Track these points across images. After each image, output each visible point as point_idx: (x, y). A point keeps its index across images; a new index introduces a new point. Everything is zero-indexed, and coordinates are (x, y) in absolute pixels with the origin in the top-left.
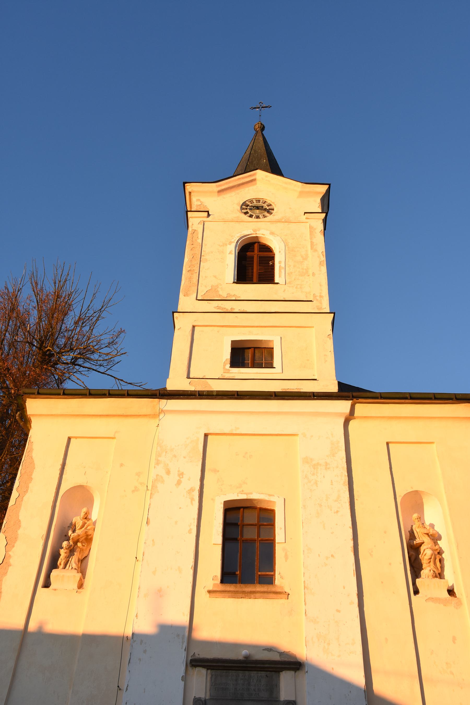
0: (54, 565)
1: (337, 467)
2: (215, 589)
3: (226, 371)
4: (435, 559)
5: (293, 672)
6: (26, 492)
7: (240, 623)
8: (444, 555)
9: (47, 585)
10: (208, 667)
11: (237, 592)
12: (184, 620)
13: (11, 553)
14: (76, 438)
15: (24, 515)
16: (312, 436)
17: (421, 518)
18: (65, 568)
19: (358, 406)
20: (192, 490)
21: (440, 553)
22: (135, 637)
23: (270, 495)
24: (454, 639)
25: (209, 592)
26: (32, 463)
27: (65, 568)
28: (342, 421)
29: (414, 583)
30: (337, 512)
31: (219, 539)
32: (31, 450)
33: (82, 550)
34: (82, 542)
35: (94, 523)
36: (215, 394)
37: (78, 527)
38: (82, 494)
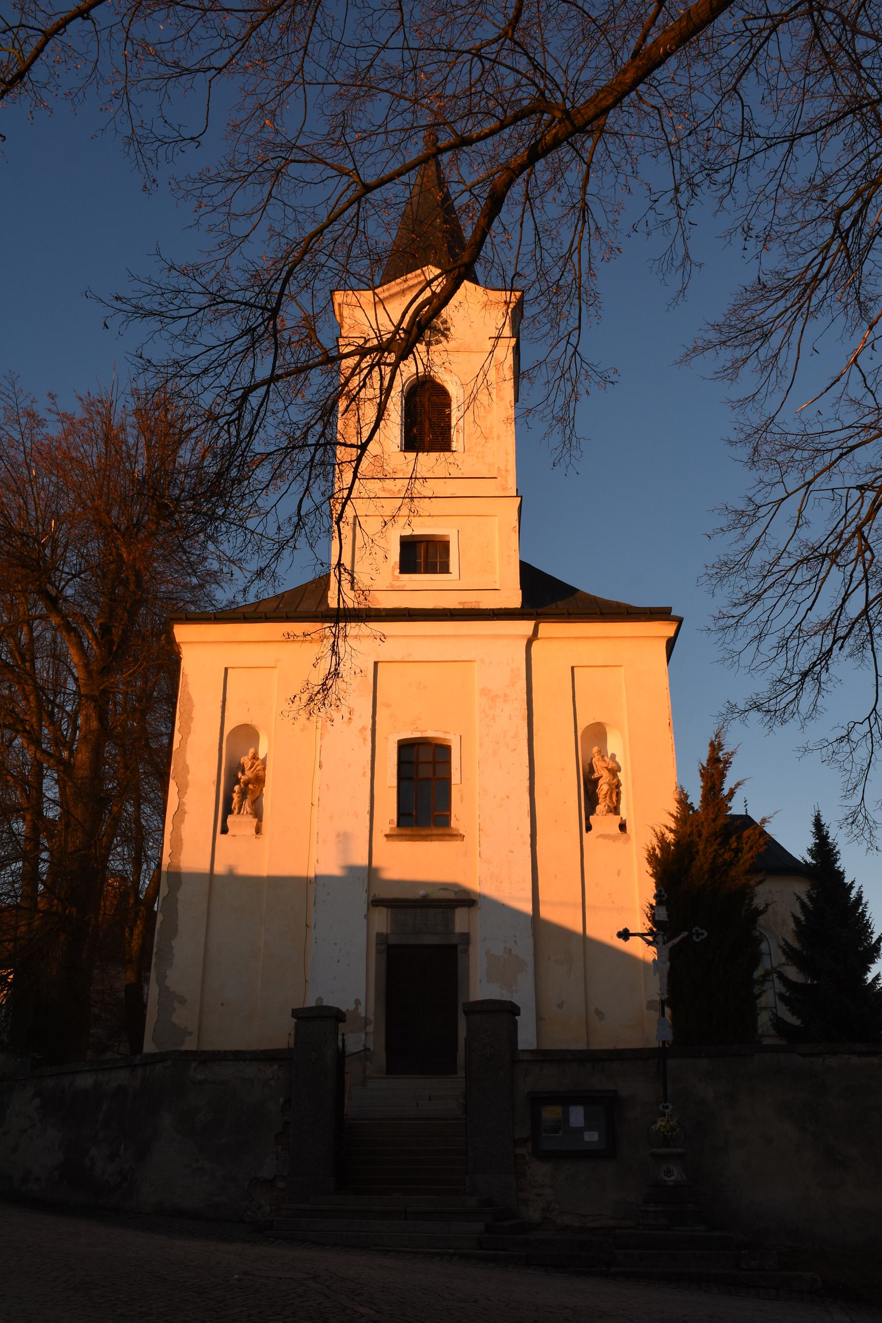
0: (228, 811)
1: (516, 699)
2: (392, 833)
3: (396, 579)
4: (612, 793)
5: (466, 909)
6: (189, 733)
7: (415, 863)
8: (621, 788)
9: (225, 831)
10: (387, 907)
11: (413, 836)
12: (365, 862)
13: (184, 800)
14: (233, 668)
15: (191, 758)
16: (491, 663)
17: (602, 753)
18: (239, 813)
19: (543, 627)
20: (364, 729)
21: (618, 785)
22: (319, 881)
23: (445, 732)
24: (619, 873)
25: (387, 836)
26: (190, 699)
27: (239, 813)
28: (524, 642)
29: (587, 819)
30: (514, 750)
31: (394, 782)
32: (186, 684)
33: (253, 791)
34: (253, 784)
35: (264, 761)
36: (383, 614)
37: (247, 767)
38: (247, 734)
